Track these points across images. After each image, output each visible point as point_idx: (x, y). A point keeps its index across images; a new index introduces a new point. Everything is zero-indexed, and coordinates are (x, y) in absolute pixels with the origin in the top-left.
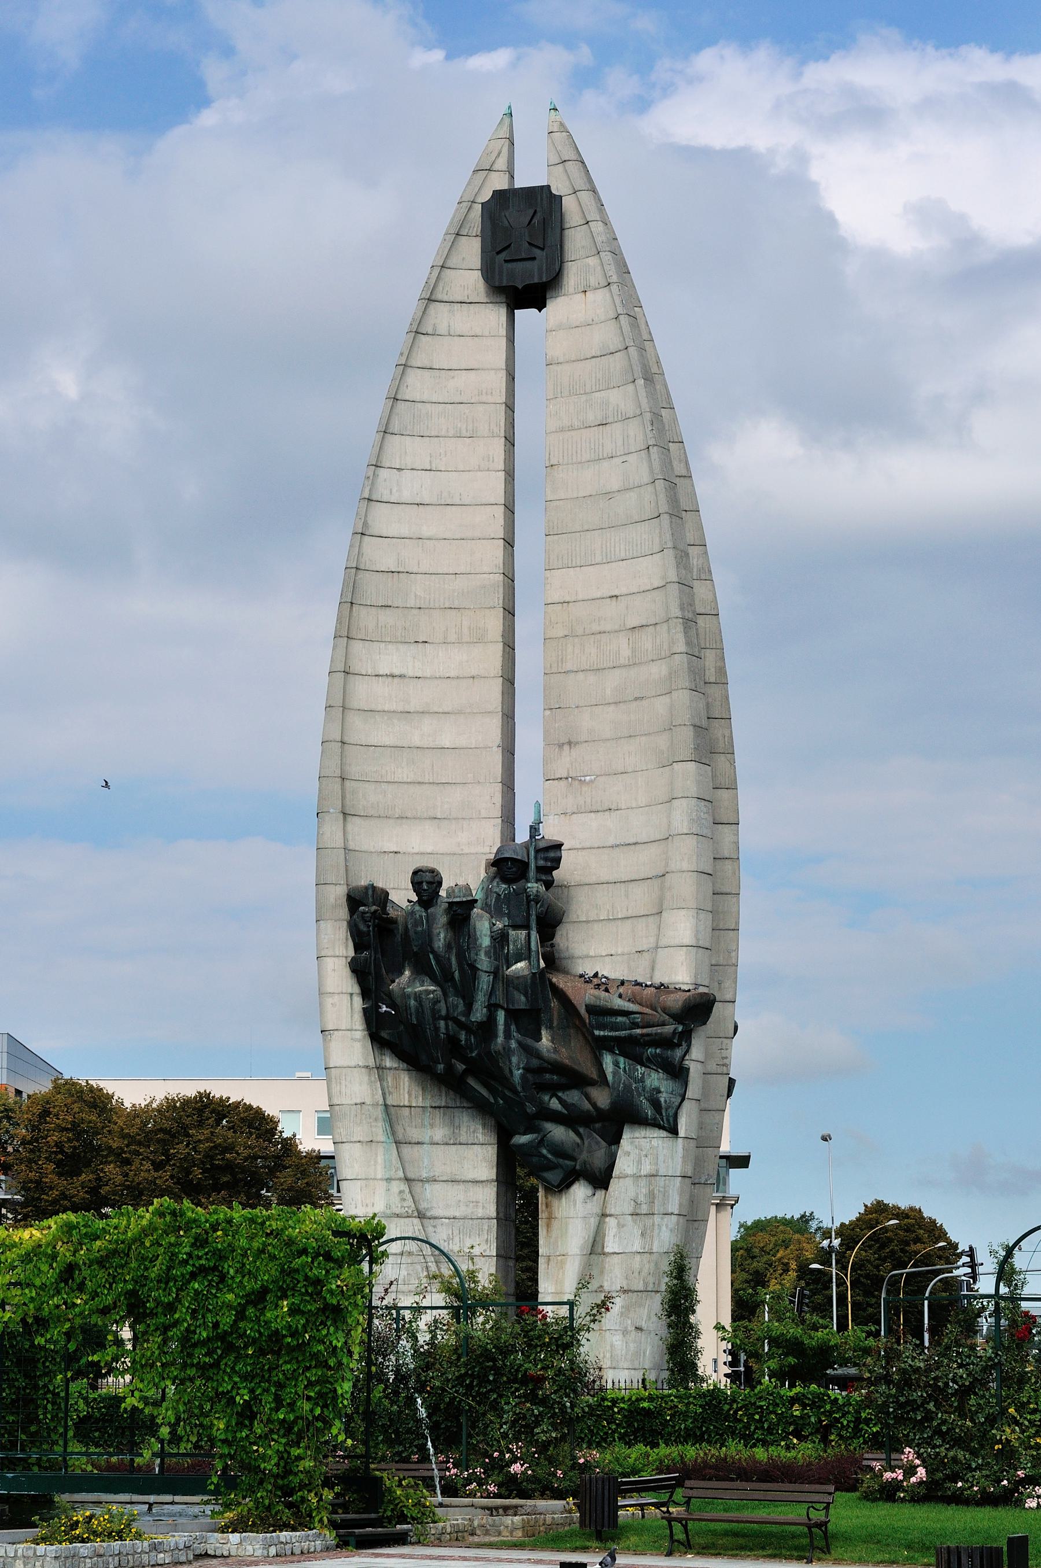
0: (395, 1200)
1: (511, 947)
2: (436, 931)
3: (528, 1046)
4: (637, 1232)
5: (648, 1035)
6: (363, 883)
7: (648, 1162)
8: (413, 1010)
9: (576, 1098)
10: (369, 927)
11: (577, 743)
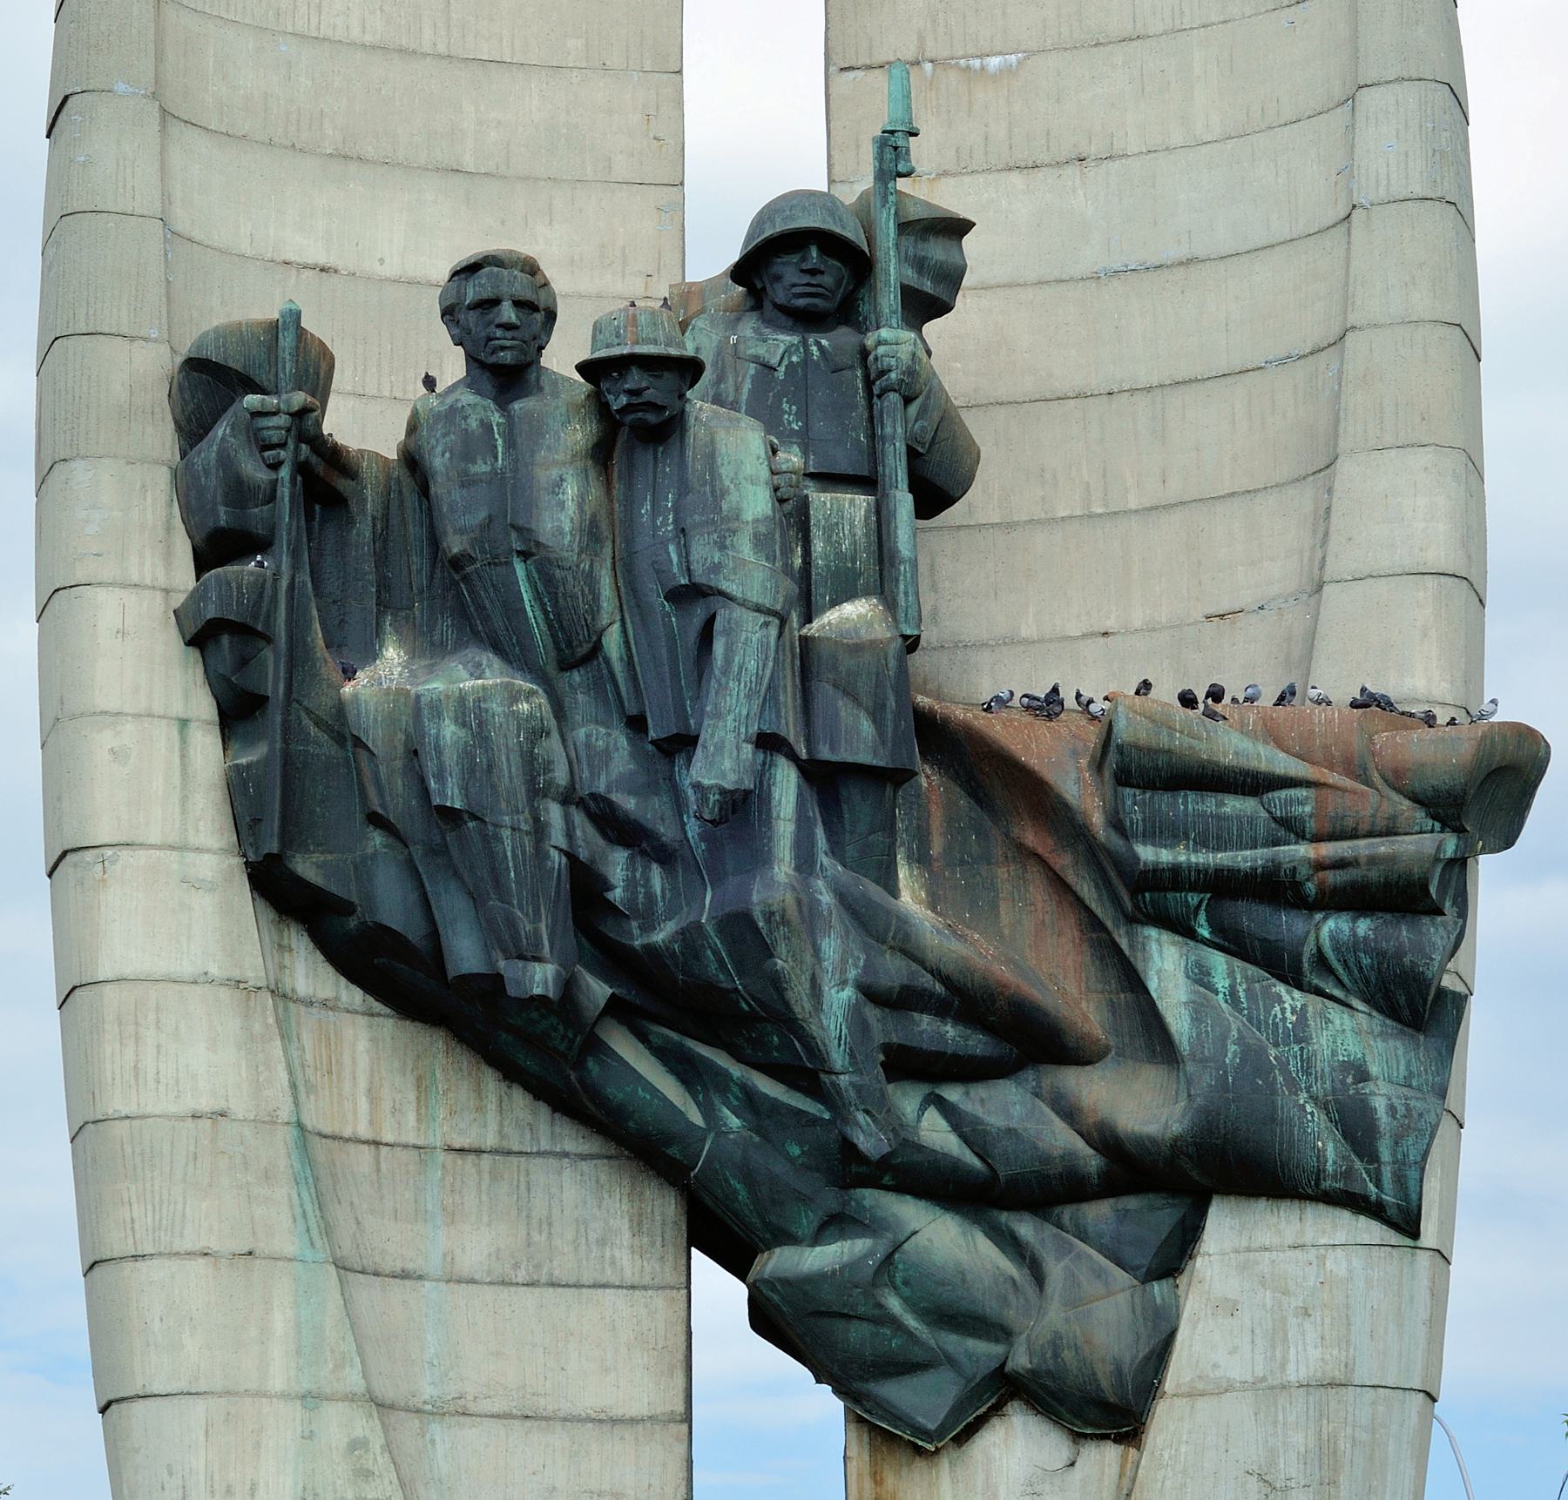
1: (818, 546)
2: (545, 476)
3: (870, 903)
5: (1340, 864)
7: (1312, 1336)
8: (450, 758)
9: (1017, 1111)
10: (275, 466)
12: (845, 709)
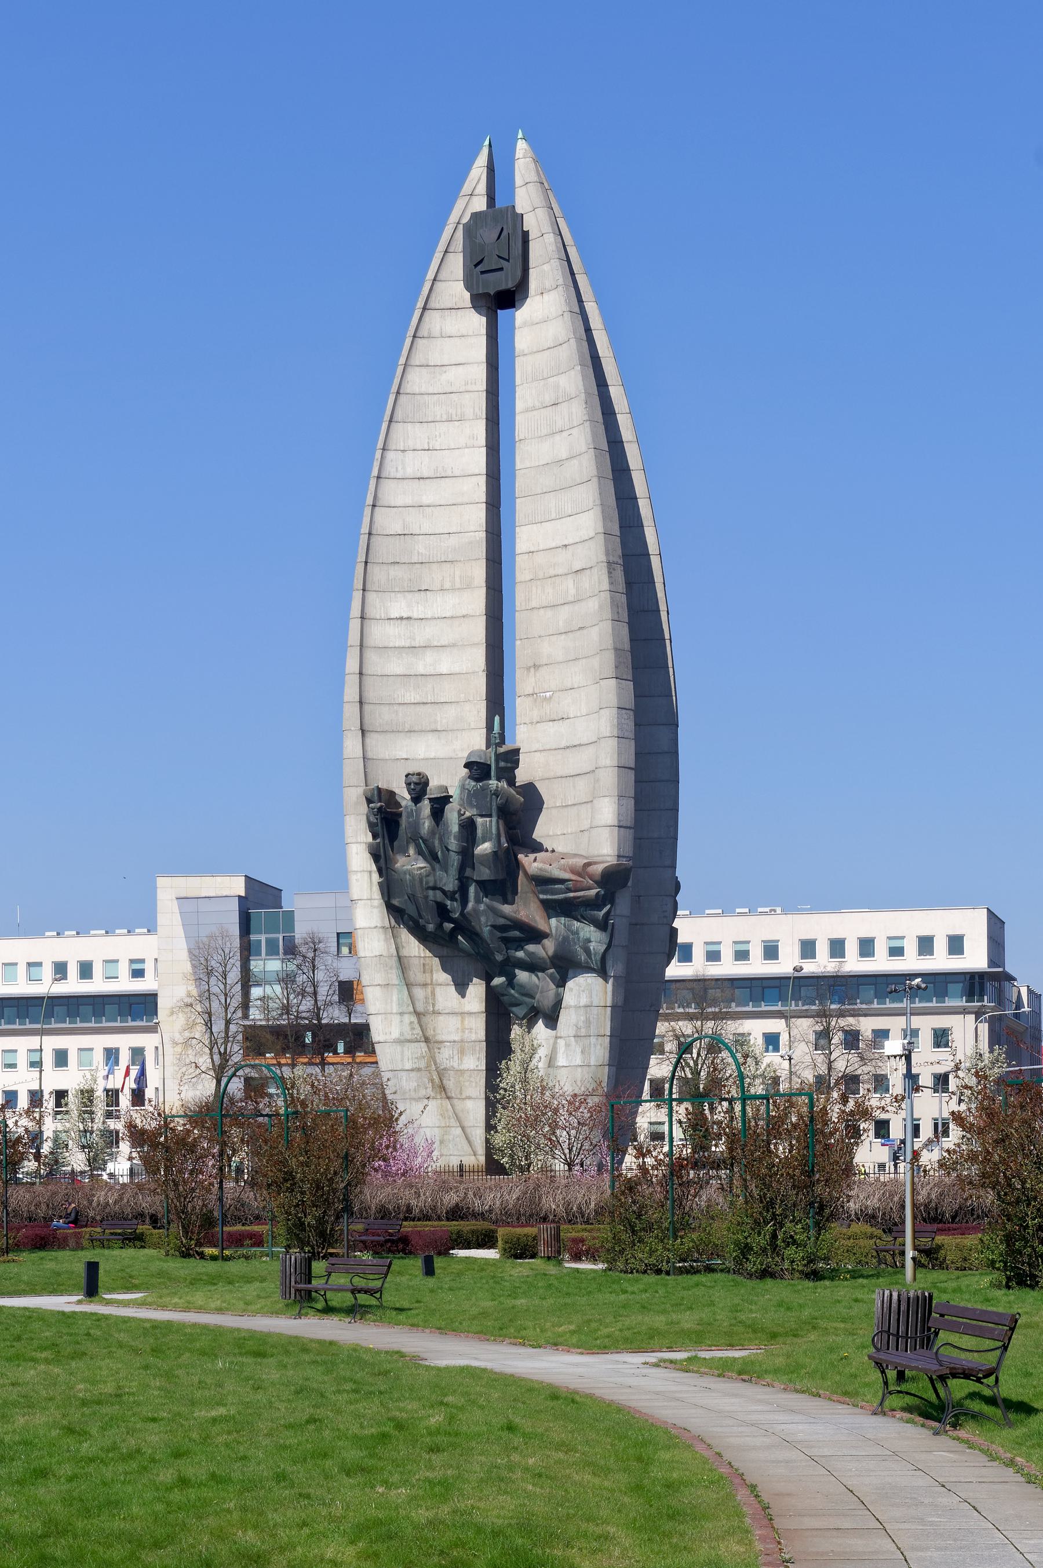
0: (407, 1028)
4: (579, 1050)
5: (579, 897)
12: (482, 868)
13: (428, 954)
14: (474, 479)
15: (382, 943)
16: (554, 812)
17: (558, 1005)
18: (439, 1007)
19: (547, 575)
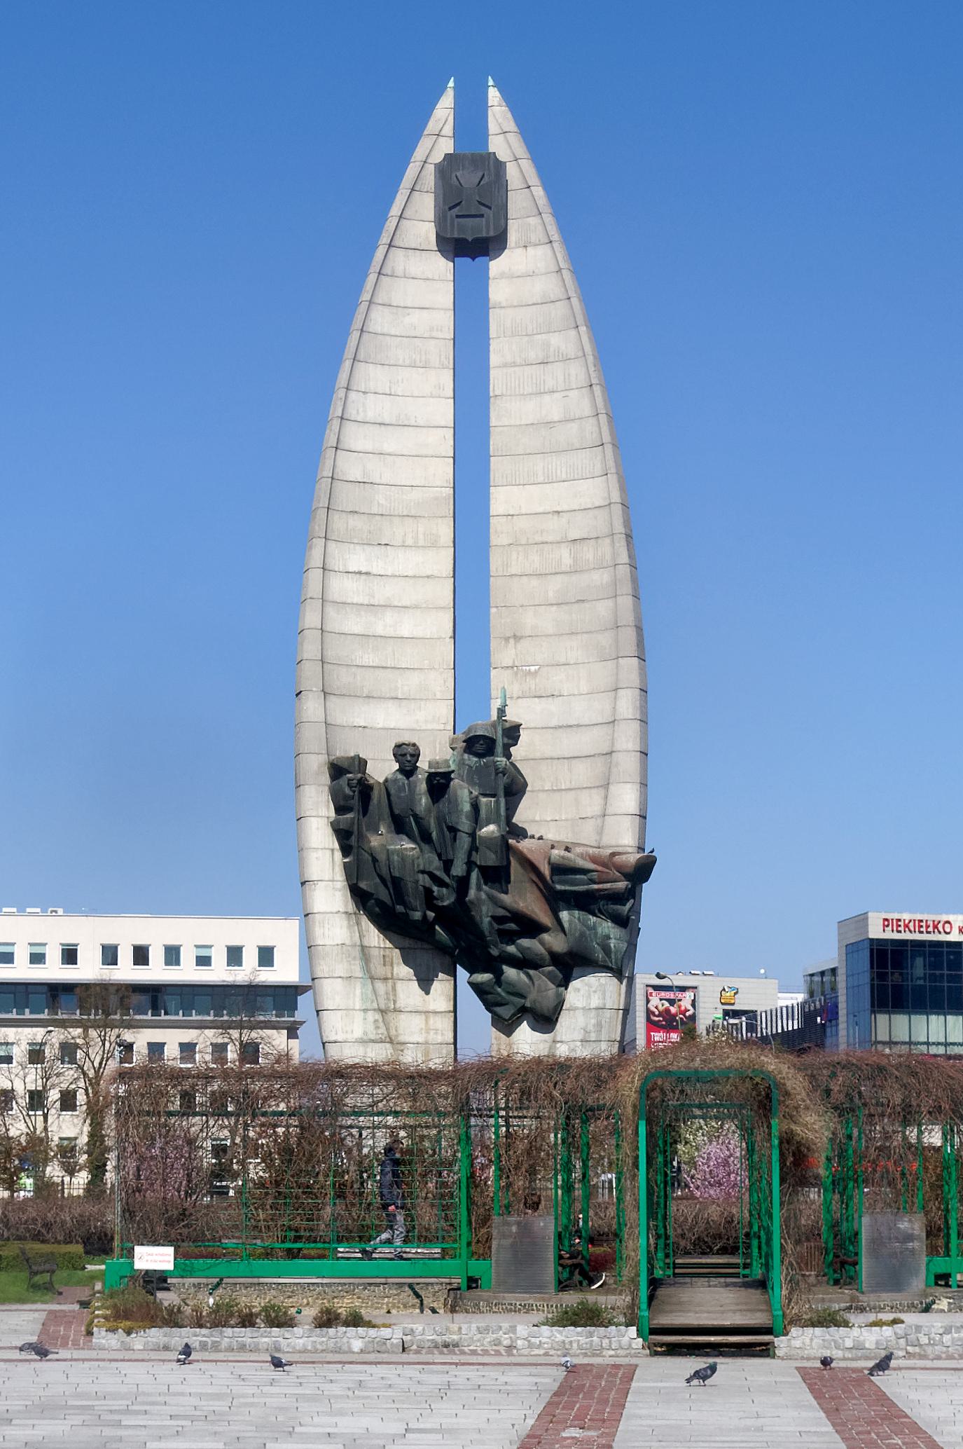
0: (371, 1028)
6: (352, 754)
11: (521, 637)
13: (388, 944)
14: (441, 431)
15: (345, 930)
16: (542, 796)
17: (559, 1006)
18: (401, 1003)
19: (531, 541)
